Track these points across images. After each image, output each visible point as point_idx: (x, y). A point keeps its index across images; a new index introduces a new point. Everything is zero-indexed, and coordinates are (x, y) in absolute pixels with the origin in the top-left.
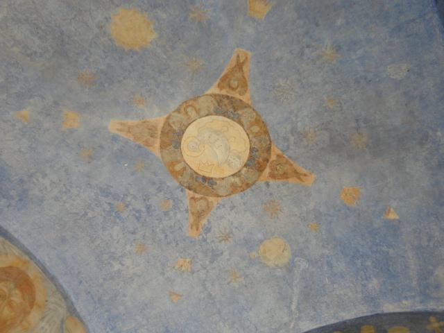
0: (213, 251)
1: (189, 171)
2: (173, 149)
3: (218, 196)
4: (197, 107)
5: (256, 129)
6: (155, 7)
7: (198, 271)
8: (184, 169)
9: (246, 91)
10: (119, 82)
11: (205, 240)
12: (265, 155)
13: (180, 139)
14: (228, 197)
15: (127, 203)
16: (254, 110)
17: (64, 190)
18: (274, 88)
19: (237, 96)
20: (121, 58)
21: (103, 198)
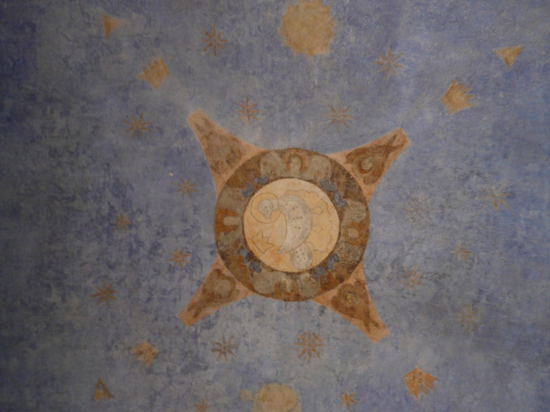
0: (196, 358)
1: (238, 234)
2: (240, 194)
3: (251, 288)
4: (307, 163)
5: (354, 233)
6: (352, 22)
7: (158, 374)
8: (235, 228)
9: (373, 182)
10: (245, 73)
11: (195, 336)
12: (344, 272)
13: (258, 188)
14: (263, 297)
15: (134, 223)
16: (367, 209)
17: (72, 149)
18: (407, 198)
19: (360, 182)
20: (269, 49)
21: (110, 194)
